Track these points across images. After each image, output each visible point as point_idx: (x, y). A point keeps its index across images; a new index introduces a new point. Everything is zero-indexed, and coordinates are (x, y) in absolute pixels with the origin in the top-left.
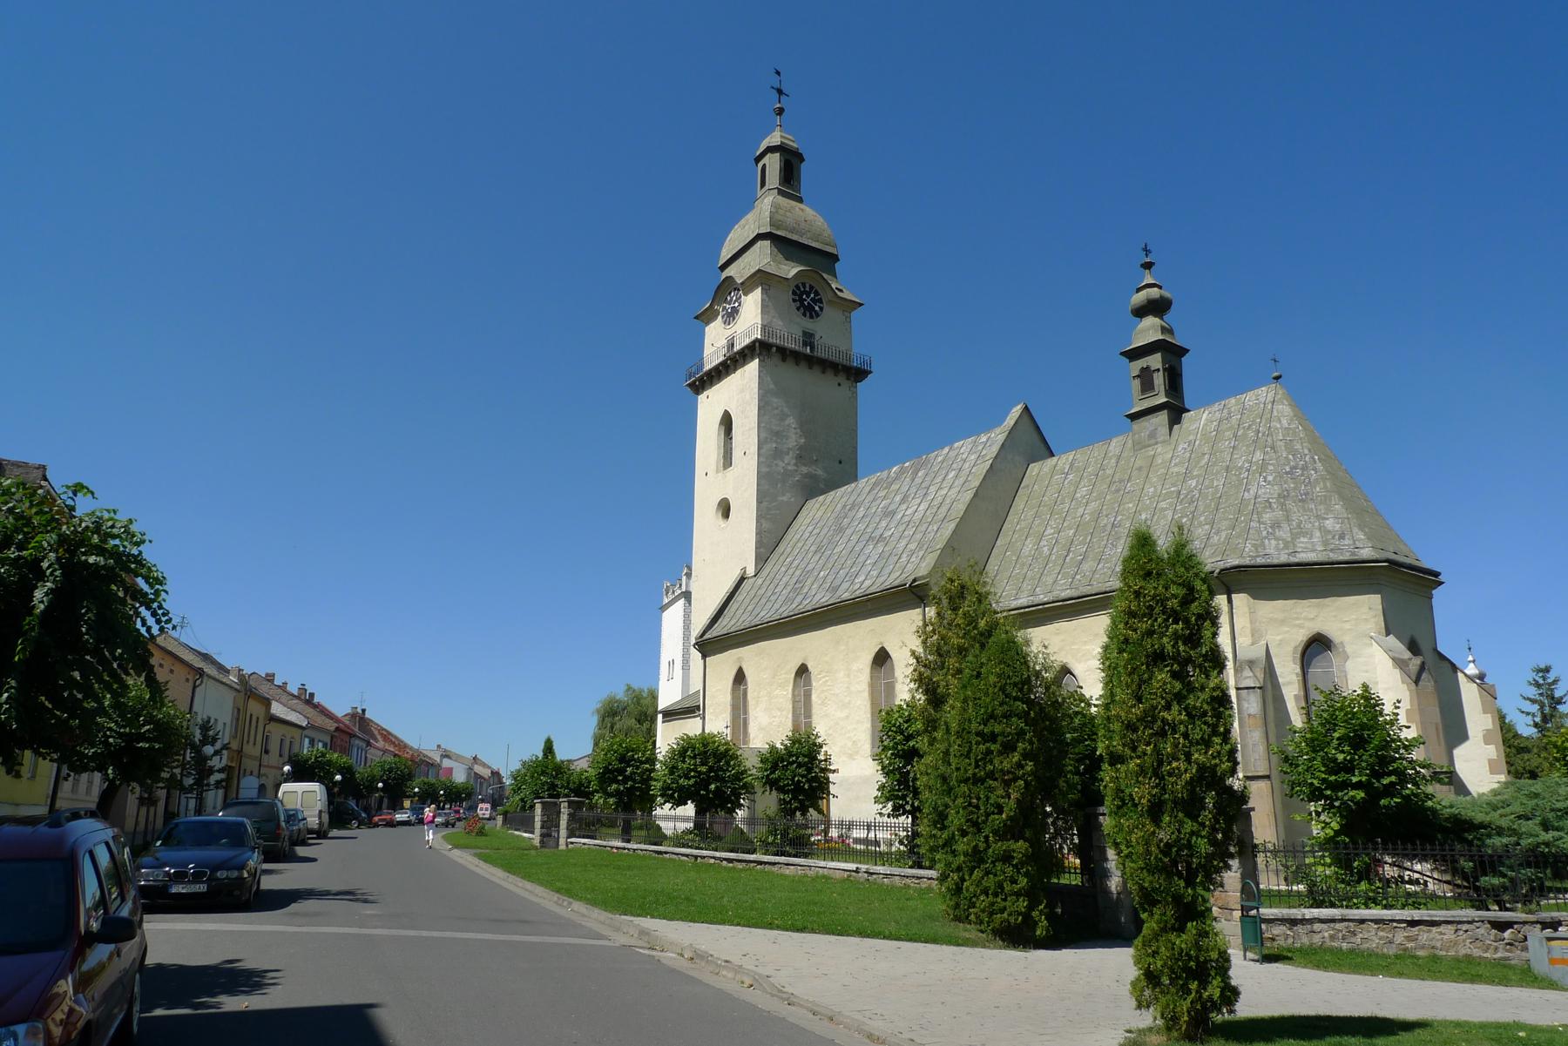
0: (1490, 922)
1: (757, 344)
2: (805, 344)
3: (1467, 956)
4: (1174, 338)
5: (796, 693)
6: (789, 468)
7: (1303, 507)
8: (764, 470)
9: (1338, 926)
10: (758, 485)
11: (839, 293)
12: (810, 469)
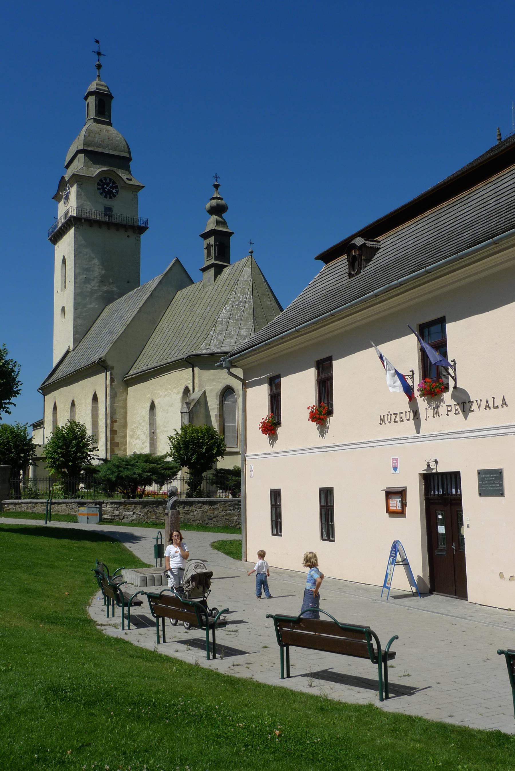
0: (77, 503)
1: (72, 219)
2: (105, 215)
3: (69, 514)
4: (227, 228)
5: (72, 415)
6: (94, 288)
7: (236, 323)
8: (79, 291)
9: (29, 505)
10: (74, 300)
11: (127, 182)
12: (109, 288)
